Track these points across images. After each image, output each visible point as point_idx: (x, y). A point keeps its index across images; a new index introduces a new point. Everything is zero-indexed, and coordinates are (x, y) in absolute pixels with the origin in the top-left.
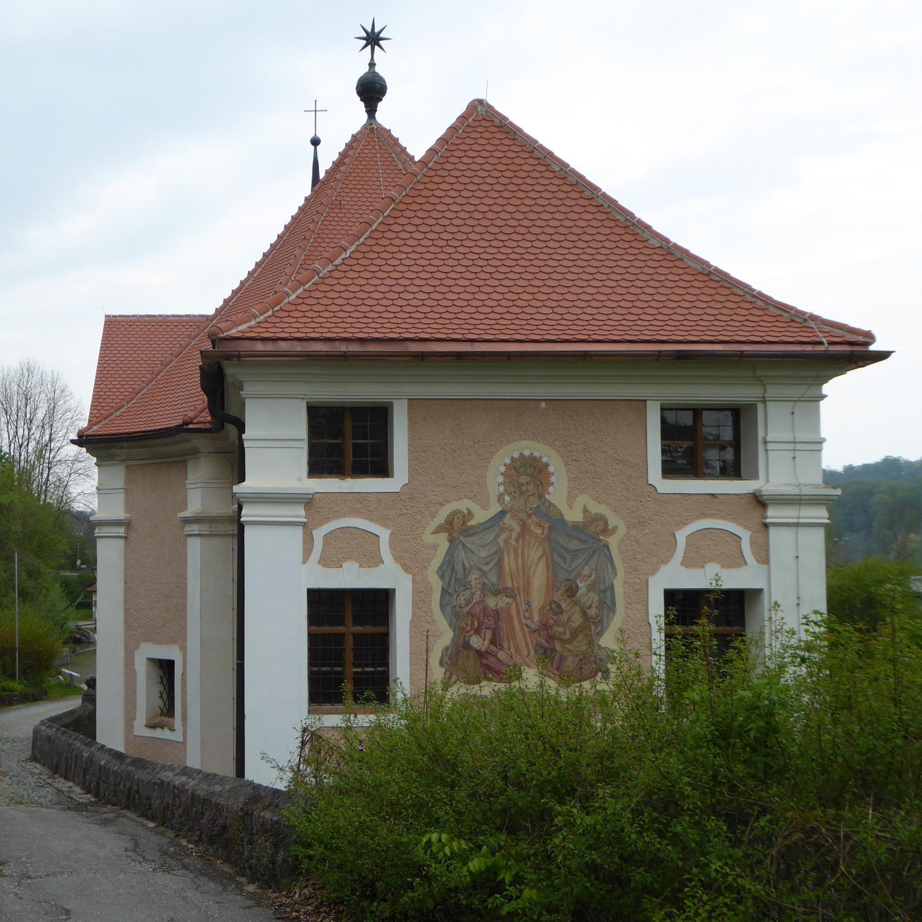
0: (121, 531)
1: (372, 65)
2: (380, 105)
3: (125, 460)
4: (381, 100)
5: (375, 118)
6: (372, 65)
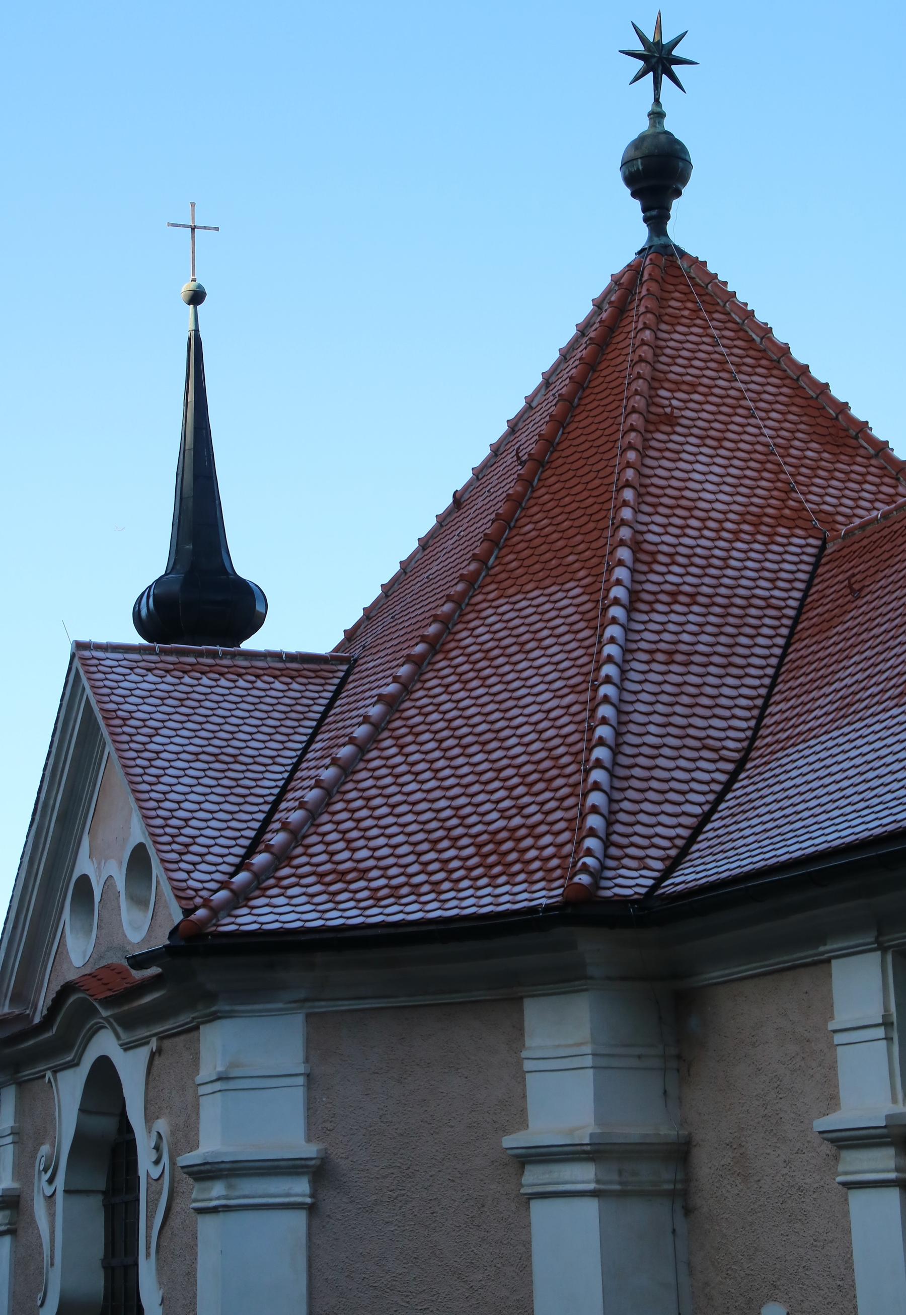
0: (300, 1188)
1: (657, 115)
2: (677, 206)
3: (306, 1000)
4: (678, 194)
5: (665, 234)
6: (657, 115)
